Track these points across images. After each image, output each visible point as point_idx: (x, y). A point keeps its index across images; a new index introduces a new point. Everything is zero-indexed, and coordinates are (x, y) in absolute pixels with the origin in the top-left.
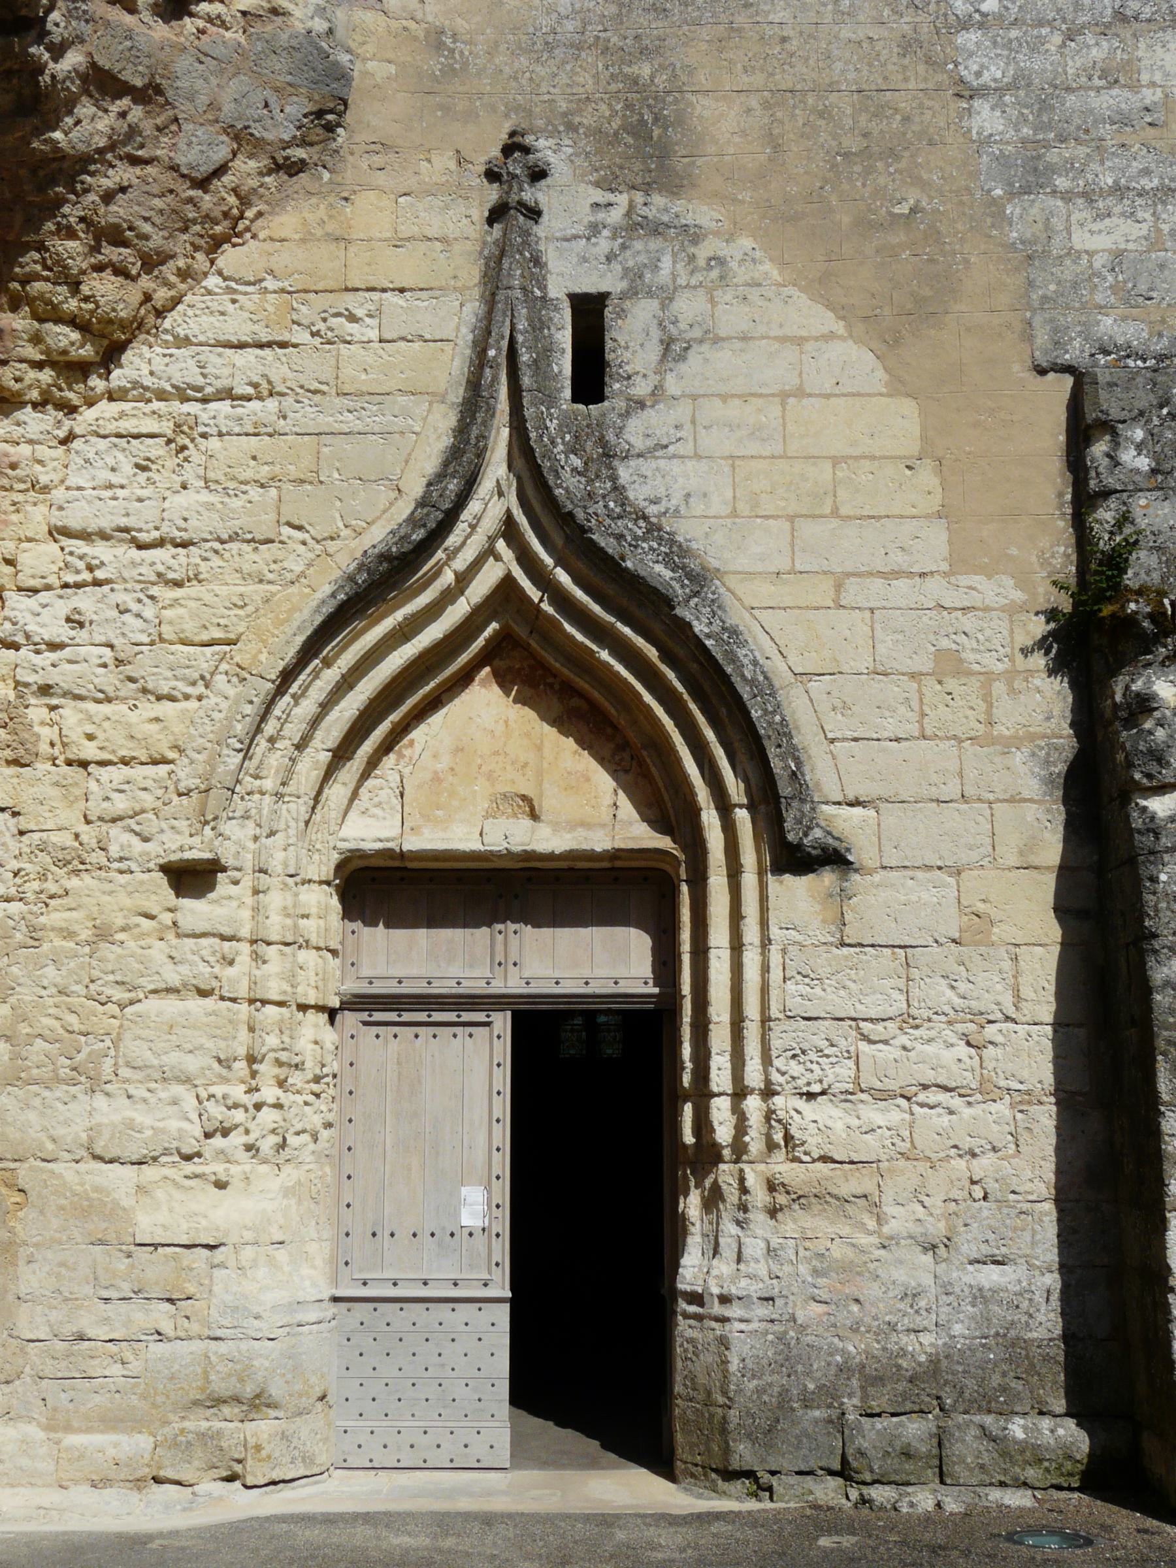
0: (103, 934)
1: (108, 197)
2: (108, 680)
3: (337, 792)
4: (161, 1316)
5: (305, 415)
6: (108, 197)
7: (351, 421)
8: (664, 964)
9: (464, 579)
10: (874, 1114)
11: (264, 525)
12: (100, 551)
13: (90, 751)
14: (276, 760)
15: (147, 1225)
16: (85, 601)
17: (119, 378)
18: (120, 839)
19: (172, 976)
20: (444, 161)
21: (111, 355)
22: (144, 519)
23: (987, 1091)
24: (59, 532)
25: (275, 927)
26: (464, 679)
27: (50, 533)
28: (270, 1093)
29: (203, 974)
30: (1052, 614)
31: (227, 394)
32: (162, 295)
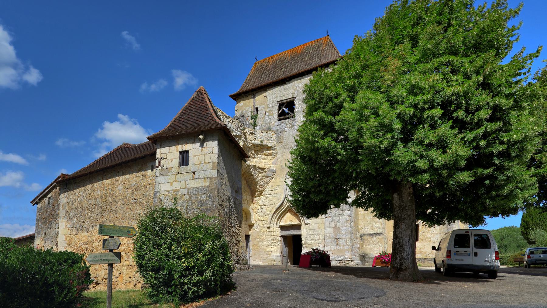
0: (264, 232)
1: (260, 183)
2: (263, 215)
3: (279, 221)
4: (269, 256)
5: (274, 195)
6: (260, 183)
7: (277, 195)
8: (167, 139)
9: (285, 206)
10: (312, 241)
11: (272, 203)
12: (262, 206)
13: (262, 220)
14: (274, 219)
15: (268, 250)
16: (262, 210)
17: (263, 194)
18: (265, 225)
19: (268, 234)
20: (282, 175)
21: (262, 192)
22: (264, 204)
23: (319, 239)
24: (260, 205)
25: (275, 230)
26: (287, 212)
27: (294, 97)
28: (275, 242)
29: (269, 234)
30: (357, 208)
31: (269, 194)
32: (265, 188)
